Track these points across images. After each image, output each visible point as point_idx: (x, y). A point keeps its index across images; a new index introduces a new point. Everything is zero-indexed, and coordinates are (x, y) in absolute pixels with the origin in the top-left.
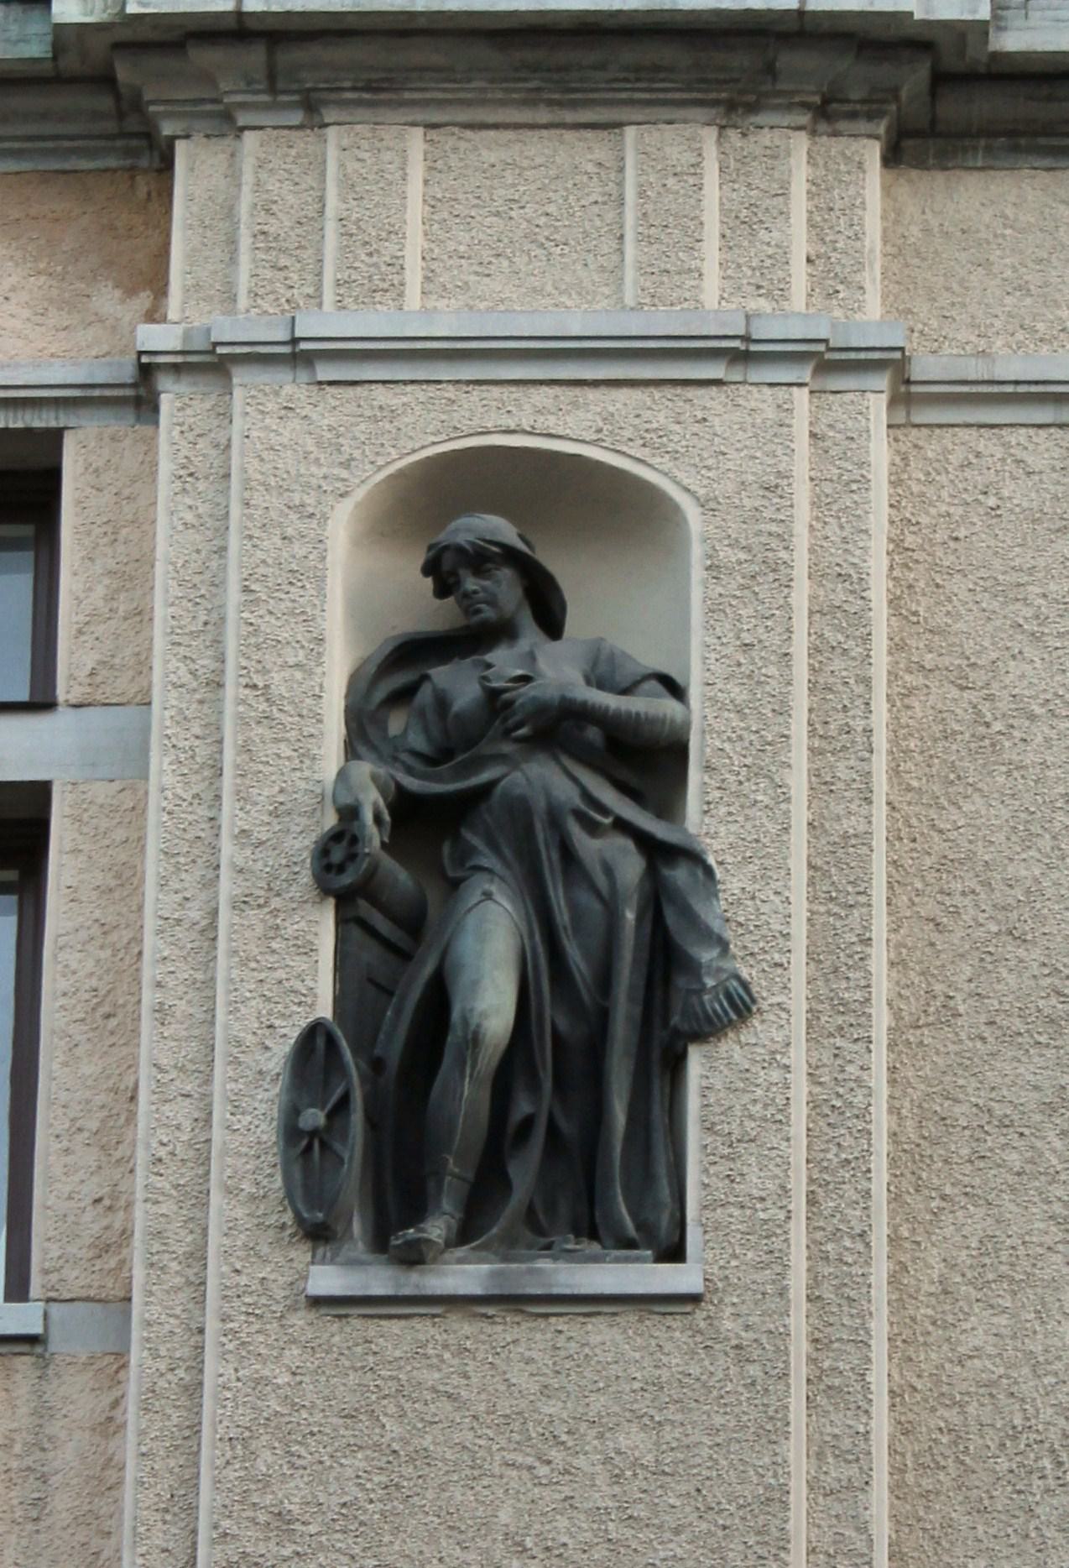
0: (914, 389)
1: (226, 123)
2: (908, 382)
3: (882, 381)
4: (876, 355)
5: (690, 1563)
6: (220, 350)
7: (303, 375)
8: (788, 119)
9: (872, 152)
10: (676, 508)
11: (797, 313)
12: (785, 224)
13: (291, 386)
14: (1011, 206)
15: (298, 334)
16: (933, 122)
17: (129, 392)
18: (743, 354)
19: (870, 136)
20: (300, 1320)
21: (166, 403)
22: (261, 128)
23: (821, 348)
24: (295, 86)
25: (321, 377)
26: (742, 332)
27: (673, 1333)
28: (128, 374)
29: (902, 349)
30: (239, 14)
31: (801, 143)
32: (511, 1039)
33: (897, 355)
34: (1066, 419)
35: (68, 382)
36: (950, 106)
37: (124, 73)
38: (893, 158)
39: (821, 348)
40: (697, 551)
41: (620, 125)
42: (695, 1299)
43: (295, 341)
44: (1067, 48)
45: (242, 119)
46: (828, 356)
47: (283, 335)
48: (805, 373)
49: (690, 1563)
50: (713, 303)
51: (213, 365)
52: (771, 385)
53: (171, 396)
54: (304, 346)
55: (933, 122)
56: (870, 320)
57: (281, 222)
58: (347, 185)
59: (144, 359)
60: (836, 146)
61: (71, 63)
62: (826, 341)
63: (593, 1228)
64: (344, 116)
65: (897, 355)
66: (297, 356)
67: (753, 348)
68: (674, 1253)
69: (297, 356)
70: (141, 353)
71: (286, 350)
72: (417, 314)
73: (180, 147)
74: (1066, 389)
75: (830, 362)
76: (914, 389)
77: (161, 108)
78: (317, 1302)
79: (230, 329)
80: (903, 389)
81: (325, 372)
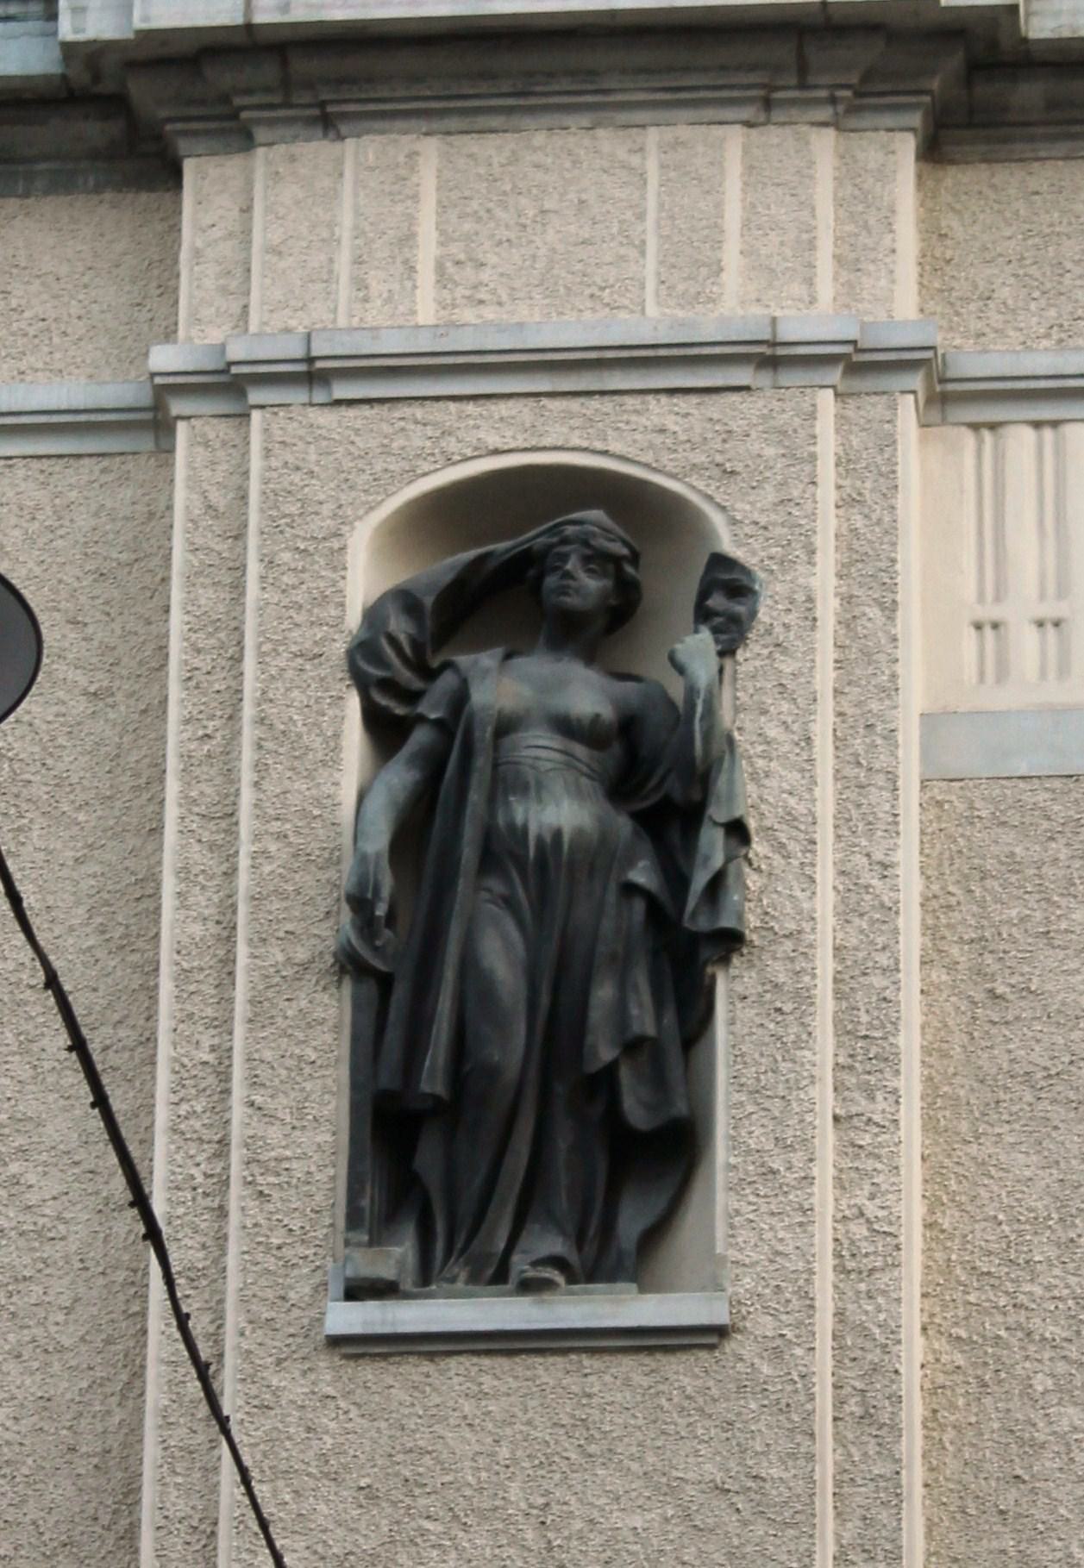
1: (240, 138)
2: (943, 381)
3: (916, 381)
5: (520, 1564)
6: (234, 370)
7: (320, 396)
9: (907, 146)
11: (814, 318)
12: (808, 221)
14: (1034, 202)
15: (314, 353)
17: (148, 416)
18: (772, 357)
20: (325, 1364)
26: (767, 336)
27: (682, 1373)
28: (145, 398)
30: (249, 27)
31: (824, 143)
32: (532, 1073)
34: (1082, 416)
36: (973, 96)
38: (933, 152)
39: (848, 349)
42: (721, 1332)
43: (310, 360)
44: (1082, 33)
46: (855, 358)
47: (299, 353)
48: (835, 375)
49: (520, 1564)
50: (733, 309)
51: (229, 385)
54: (319, 365)
57: (318, 241)
59: (158, 380)
60: (773, 136)
61: (80, 77)
62: (854, 342)
67: (781, 351)
69: (312, 374)
70: (153, 375)
71: (301, 368)
74: (1081, 383)
75: (860, 365)
76: (950, 387)
77: (179, 126)
78: (336, 1342)
81: (342, 391)
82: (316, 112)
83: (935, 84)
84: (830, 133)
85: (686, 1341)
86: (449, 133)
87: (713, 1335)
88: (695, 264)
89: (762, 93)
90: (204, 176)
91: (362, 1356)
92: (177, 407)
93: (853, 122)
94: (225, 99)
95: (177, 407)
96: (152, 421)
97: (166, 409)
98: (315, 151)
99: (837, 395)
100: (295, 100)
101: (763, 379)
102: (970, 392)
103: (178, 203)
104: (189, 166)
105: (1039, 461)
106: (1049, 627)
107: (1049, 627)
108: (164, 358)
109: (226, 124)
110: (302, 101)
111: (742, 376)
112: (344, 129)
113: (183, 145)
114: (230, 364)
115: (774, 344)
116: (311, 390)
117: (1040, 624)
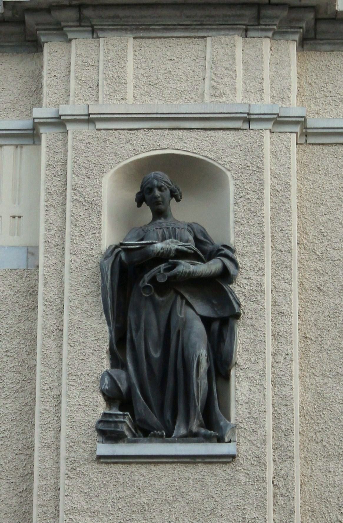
0: (309, 131)
2: (307, 128)
3: (298, 129)
4: (294, 119)
6: (62, 118)
7: (91, 127)
9: (293, 47)
10: (224, 173)
11: (262, 106)
12: (258, 70)
13: (86, 130)
14: (329, 63)
19: (265, 37)
21: (43, 137)
23: (275, 116)
25: (97, 127)
26: (248, 112)
27: (220, 471)
29: (304, 117)
33: (303, 119)
34: (342, 141)
37: (29, 19)
39: (275, 116)
40: (232, 188)
41: (206, 37)
42: (233, 457)
45: (70, 36)
47: (86, 113)
48: (270, 125)
50: (238, 101)
51: (60, 122)
52: (105, 129)
53: (47, 135)
54: (91, 116)
56: (294, 108)
58: (78, 56)
59: (36, 121)
61: (9, 14)
62: (278, 114)
65: (303, 119)
66: (89, 120)
67: (252, 117)
69: (89, 120)
70: (34, 119)
71: (86, 117)
72: (131, 105)
73: (46, 45)
74: (342, 130)
75: (278, 121)
76: (309, 131)
78: (100, 457)
79: (66, 110)
80: (304, 131)
81: (99, 125)
82: (90, 29)
83: (304, 25)
84: (268, 40)
85: (131, 460)
87: (229, 459)
89: (244, 27)
90: (52, 51)
96: (31, 135)
99: (271, 132)
100: (83, 24)
105: (330, 158)
106: (17, 218)
107: (17, 218)
108: (37, 113)
110: (85, 24)
111: (238, 124)
112: (100, 34)
114: (61, 116)
115: (249, 114)
117: (14, 217)
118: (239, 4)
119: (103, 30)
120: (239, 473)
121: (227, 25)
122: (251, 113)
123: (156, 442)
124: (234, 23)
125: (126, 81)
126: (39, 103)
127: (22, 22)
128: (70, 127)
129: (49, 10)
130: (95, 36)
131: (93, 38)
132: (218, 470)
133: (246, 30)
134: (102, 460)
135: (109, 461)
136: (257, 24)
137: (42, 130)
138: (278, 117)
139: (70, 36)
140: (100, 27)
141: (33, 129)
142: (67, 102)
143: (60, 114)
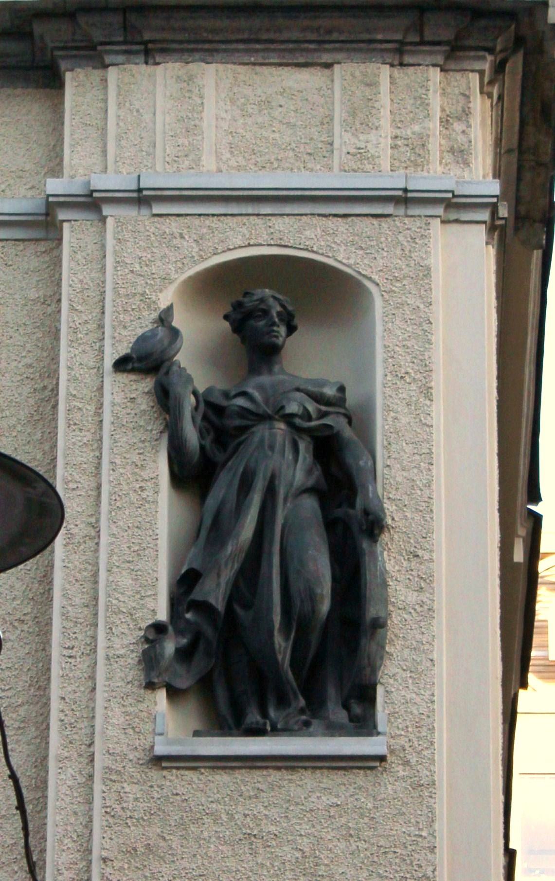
6: (95, 195)
7: (145, 211)
8: (429, 60)
12: (433, 124)
13: (129, 213)
15: (141, 186)
16: (125, 13)
17: (40, 218)
18: (404, 199)
22: (419, 65)
23: (450, 195)
24: (139, 39)
31: (385, 71)
35: (12, 212)
37: (38, 28)
39: (450, 195)
42: (382, 759)
43: (140, 190)
45: (108, 59)
47: (134, 187)
48: (440, 211)
51: (92, 203)
54: (145, 193)
55: (125, 13)
59: (51, 199)
62: (453, 192)
63: (313, 716)
64: (120, 58)
66: (141, 198)
67: (410, 195)
68: (364, 724)
69: (141, 198)
70: (48, 196)
71: (135, 195)
79: (102, 182)
81: (157, 209)
85: (259, 764)
86: (254, 64)
88: (415, 151)
90: (77, 84)
91: (352, 768)
92: (62, 215)
93: (452, 65)
94: (145, 43)
95: (62, 215)
96: (43, 225)
97: (54, 217)
98: (140, 71)
101: (401, 211)
102: (257, 196)
103: (62, 95)
104: (68, 76)
108: (55, 186)
109: (91, 53)
111: (389, 209)
113: (63, 65)
115: (405, 190)
116: (139, 209)
118: (353, 7)
119: (163, 51)
120: (391, 784)
121: (363, 46)
122: (409, 188)
123: (340, 736)
124: (353, 37)
125: (194, 135)
126: (56, 171)
127: (30, 35)
128: (107, 210)
129: (70, 15)
130: (151, 61)
131: (146, 63)
132: (360, 778)
133: (400, 52)
134: (164, 764)
135: (334, 764)
136: (417, 39)
137: (62, 215)
138: (454, 196)
139: (158, 60)
140: (159, 46)
141: (47, 214)
142: (105, 170)
143: (92, 188)
